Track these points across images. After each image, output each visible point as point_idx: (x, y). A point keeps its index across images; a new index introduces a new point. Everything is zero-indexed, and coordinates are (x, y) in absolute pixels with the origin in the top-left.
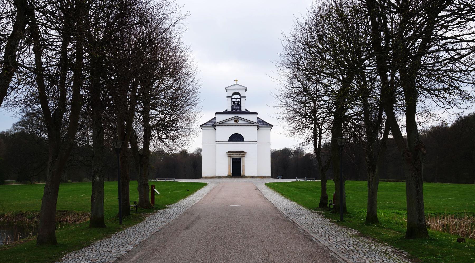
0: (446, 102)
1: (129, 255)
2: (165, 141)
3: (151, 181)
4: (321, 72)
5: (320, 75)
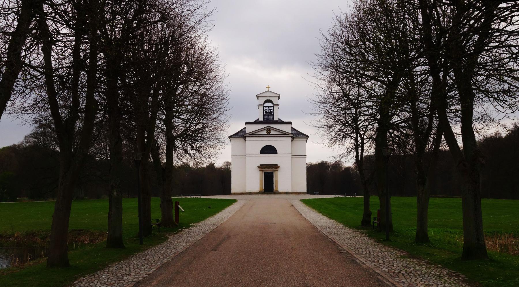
0: (506, 106)
1: (150, 278)
2: (190, 152)
3: (175, 198)
4: (364, 74)
5: (362, 78)
